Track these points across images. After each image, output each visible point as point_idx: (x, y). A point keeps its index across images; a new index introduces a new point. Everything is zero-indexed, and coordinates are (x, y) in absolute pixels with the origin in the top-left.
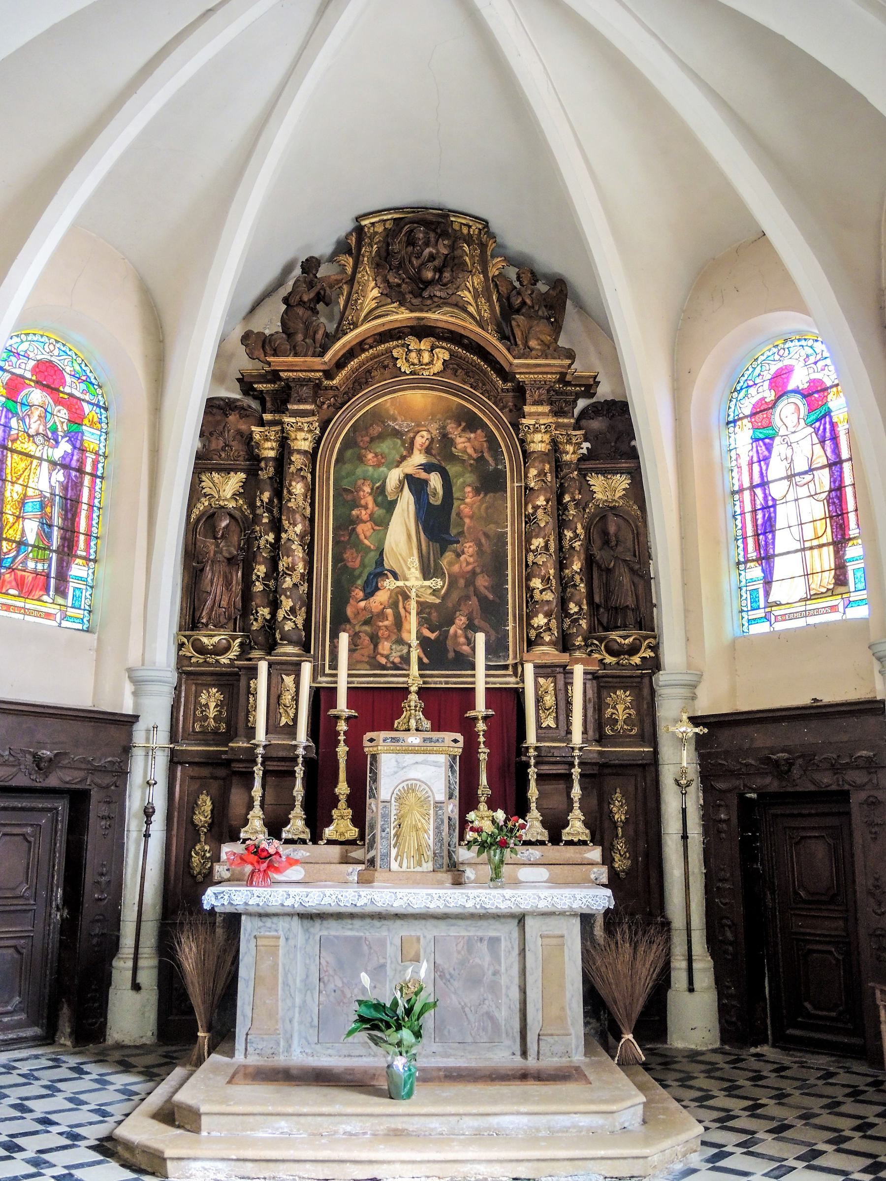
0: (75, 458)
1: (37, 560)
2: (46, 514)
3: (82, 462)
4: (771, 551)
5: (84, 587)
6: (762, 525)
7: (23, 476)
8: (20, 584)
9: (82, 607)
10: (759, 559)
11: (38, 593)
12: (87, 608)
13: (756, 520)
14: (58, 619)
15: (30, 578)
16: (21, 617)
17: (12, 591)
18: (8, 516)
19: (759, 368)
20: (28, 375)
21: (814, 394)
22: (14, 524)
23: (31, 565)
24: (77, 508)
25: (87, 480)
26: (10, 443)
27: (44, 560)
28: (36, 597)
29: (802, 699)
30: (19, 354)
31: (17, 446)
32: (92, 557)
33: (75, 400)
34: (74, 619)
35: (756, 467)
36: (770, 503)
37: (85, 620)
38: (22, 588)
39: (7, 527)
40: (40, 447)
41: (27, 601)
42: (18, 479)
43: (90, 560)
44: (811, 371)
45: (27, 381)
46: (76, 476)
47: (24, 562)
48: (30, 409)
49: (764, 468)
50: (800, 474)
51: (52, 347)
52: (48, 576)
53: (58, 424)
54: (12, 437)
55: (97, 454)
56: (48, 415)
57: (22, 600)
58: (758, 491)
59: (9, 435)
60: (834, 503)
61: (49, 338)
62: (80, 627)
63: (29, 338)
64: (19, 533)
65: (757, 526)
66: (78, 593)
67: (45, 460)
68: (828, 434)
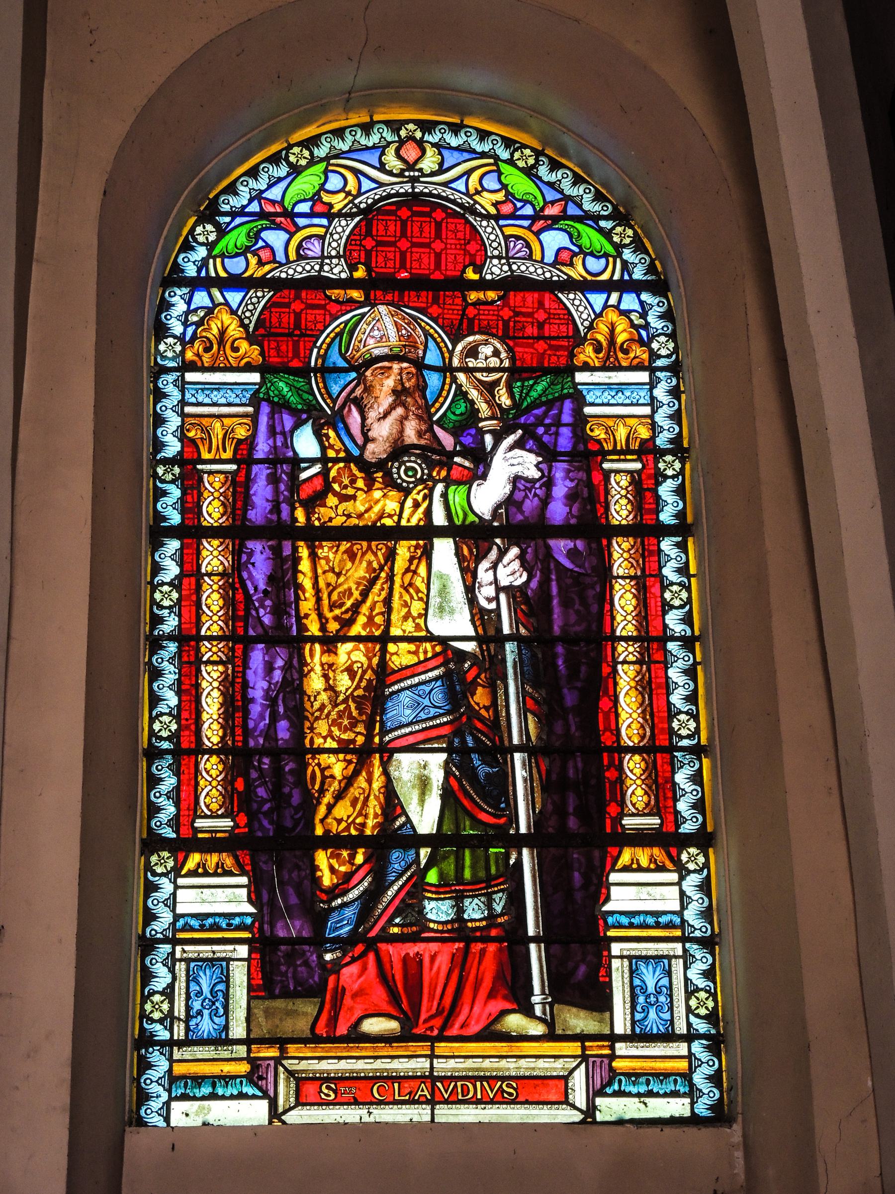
0: (560, 490)
1: (454, 889)
2: (472, 713)
3: (590, 497)
5: (678, 948)
7: (365, 609)
8: (404, 996)
9: (681, 1028)
11: (477, 1013)
12: (702, 1027)
14: (579, 1098)
15: (443, 962)
16: (420, 1114)
17: (373, 1025)
18: (326, 759)
20: (338, 270)
22: (349, 781)
23: (438, 911)
24: (596, 665)
25: (621, 556)
26: (300, 515)
27: (489, 880)
28: (474, 1028)
29: (435, 754)
30: (291, 215)
31: (332, 512)
32: (688, 828)
33: (531, 298)
34: (650, 1081)
37: (698, 1078)
38: (416, 1007)
39: (328, 798)
40: (417, 495)
41: (442, 1047)
42: (351, 622)
43: (687, 841)
45: (335, 293)
46: (572, 554)
47: (411, 904)
48: (361, 378)
51: (411, 152)
52: (515, 937)
53: (474, 394)
54: (306, 492)
55: (647, 450)
56: (433, 380)
57: (423, 1048)
59: (295, 484)
61: (395, 126)
62: (679, 1107)
63: (321, 152)
64: (374, 806)
66: (650, 977)
67: (442, 532)
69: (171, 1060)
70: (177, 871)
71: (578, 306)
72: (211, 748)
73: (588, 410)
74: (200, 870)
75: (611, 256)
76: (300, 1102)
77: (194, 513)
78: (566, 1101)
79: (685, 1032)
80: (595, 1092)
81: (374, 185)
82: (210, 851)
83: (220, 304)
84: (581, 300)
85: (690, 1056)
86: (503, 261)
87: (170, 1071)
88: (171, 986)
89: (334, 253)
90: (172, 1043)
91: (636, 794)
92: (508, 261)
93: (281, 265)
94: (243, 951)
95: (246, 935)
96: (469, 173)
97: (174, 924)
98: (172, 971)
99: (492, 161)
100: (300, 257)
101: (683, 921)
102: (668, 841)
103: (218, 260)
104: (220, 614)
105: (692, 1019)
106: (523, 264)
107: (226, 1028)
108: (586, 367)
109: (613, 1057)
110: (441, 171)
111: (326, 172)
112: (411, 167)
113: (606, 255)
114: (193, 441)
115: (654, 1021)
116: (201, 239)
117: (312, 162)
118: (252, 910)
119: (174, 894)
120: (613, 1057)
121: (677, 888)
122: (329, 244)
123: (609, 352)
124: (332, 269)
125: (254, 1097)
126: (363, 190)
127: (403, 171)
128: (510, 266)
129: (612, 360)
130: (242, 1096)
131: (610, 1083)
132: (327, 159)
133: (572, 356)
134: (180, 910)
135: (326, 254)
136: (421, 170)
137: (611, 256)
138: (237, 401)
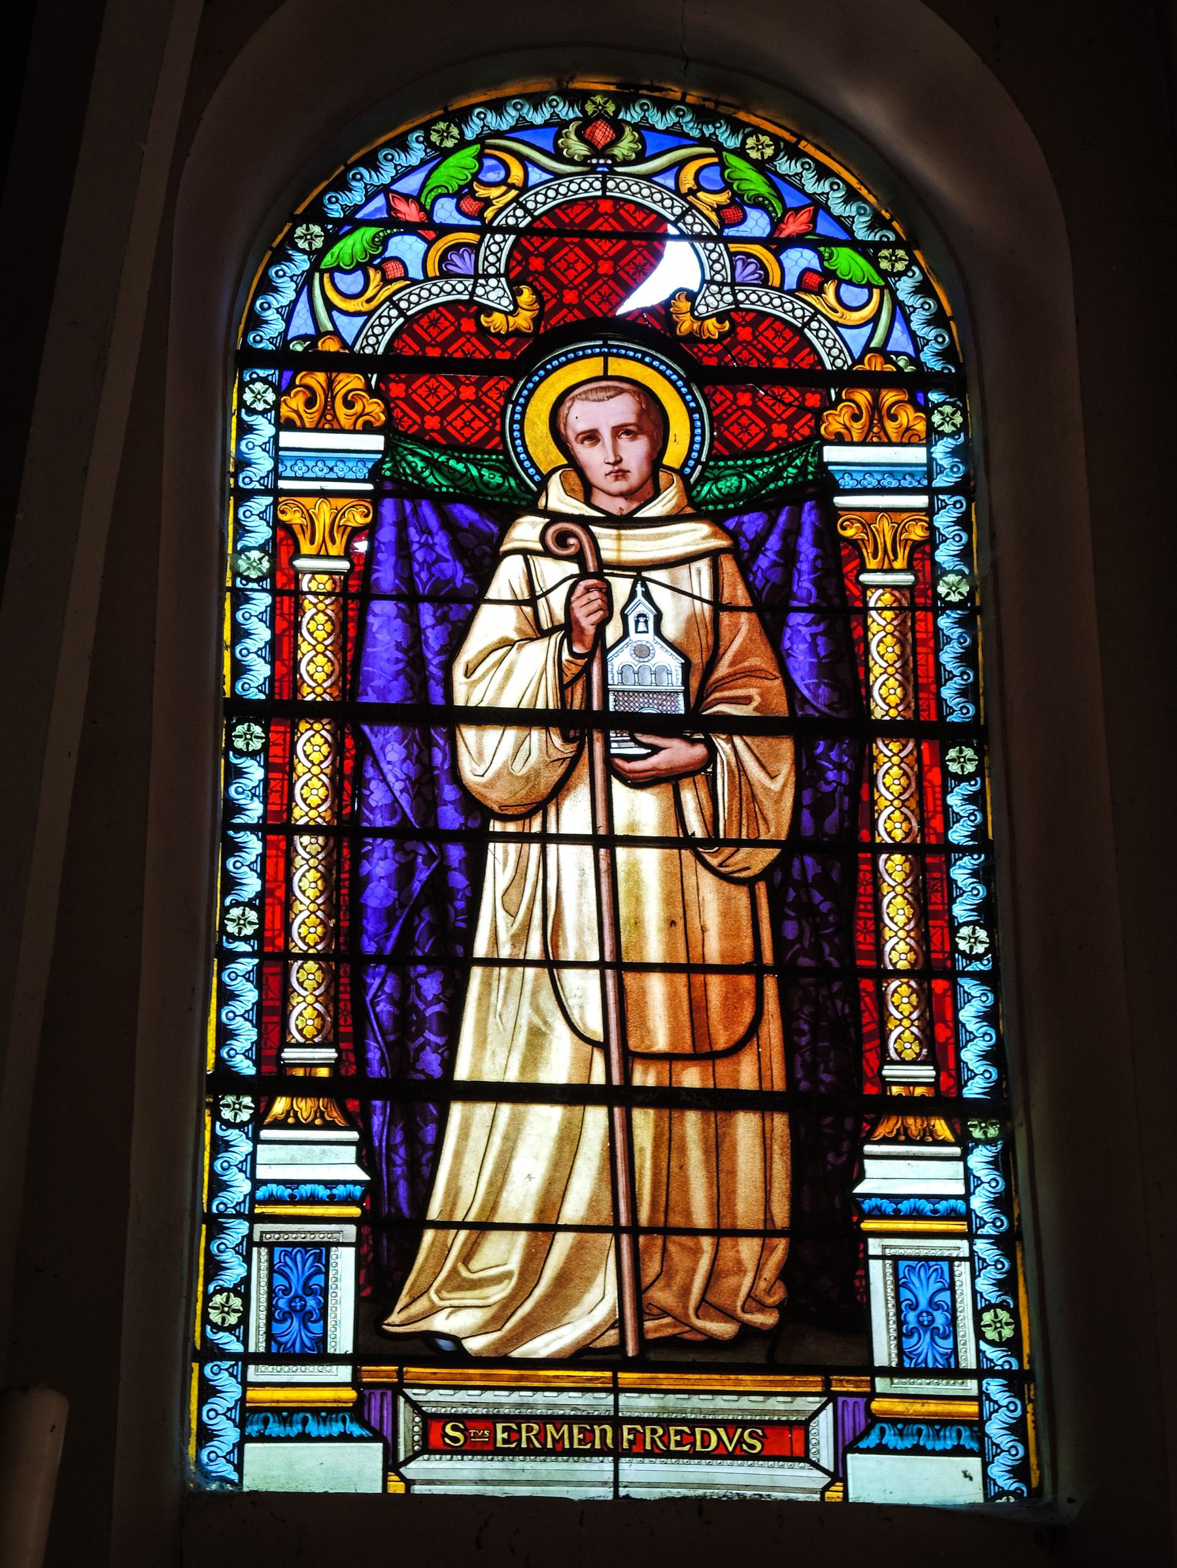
4: (432, 1061)
6: (389, 915)
9: (968, 1360)
10: (345, 1095)
13: (359, 883)
19: (466, 158)
21: (751, 381)
34: (921, 1435)
35: (384, 624)
36: (451, 818)
44: (747, 272)
49: (433, 638)
50: (634, 724)
51: (602, 133)
58: (392, 751)
60: (806, 910)
65: (357, 910)
68: (804, 585)
69: (245, 1384)
70: (259, 1120)
71: (830, 349)
72: (305, 953)
73: (839, 501)
74: (291, 1120)
75: (877, 287)
76: (427, 1448)
77: (284, 772)
78: (805, 1457)
79: (974, 1366)
80: (845, 1446)
81: (547, 176)
82: (304, 1095)
83: (328, 333)
84: (835, 340)
85: (981, 1397)
86: (726, 289)
87: (243, 1399)
88: (246, 1281)
89: (492, 270)
90: (247, 1359)
91: (902, 1035)
92: (733, 290)
93: (415, 282)
94: (350, 1232)
95: (355, 1211)
96: (681, 164)
97: (252, 1194)
98: (248, 1260)
99: (711, 150)
100: (445, 275)
101: (969, 1211)
102: (945, 1101)
103: (326, 276)
104: (327, 642)
105: (983, 1346)
106: (754, 292)
107: (323, 1339)
108: (840, 440)
109: (873, 1395)
110: (641, 158)
111: (480, 157)
112: (597, 152)
113: (870, 286)
114: (288, 527)
115: (924, 1348)
116: (302, 244)
117: (463, 144)
118: (363, 1176)
119: (253, 1154)
120: (873, 1395)
121: (961, 1164)
122: (486, 258)
123: (871, 418)
124: (487, 293)
125: (361, 1439)
126: (530, 183)
127: (586, 157)
128: (734, 295)
129: (875, 430)
130: (345, 1437)
131: (866, 1433)
132: (479, 139)
133: (819, 421)
134: (262, 1173)
135: (481, 272)
136: (613, 157)
137: (877, 287)
138: (351, 476)
